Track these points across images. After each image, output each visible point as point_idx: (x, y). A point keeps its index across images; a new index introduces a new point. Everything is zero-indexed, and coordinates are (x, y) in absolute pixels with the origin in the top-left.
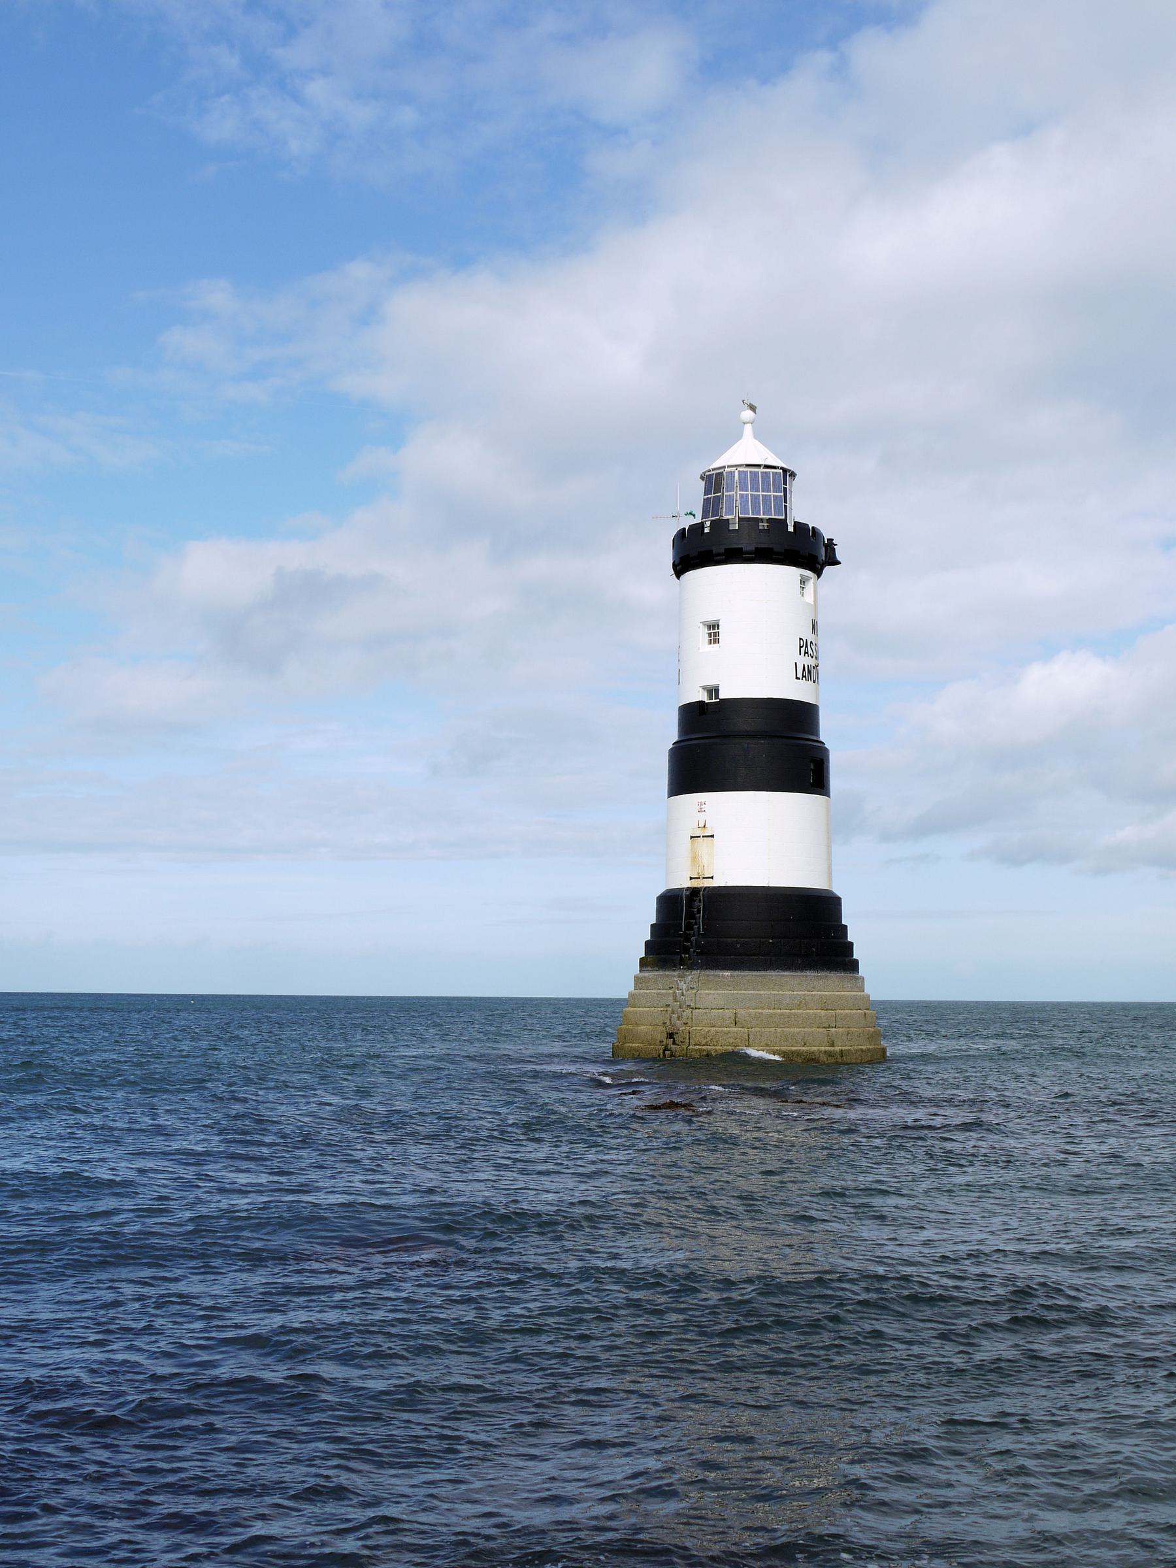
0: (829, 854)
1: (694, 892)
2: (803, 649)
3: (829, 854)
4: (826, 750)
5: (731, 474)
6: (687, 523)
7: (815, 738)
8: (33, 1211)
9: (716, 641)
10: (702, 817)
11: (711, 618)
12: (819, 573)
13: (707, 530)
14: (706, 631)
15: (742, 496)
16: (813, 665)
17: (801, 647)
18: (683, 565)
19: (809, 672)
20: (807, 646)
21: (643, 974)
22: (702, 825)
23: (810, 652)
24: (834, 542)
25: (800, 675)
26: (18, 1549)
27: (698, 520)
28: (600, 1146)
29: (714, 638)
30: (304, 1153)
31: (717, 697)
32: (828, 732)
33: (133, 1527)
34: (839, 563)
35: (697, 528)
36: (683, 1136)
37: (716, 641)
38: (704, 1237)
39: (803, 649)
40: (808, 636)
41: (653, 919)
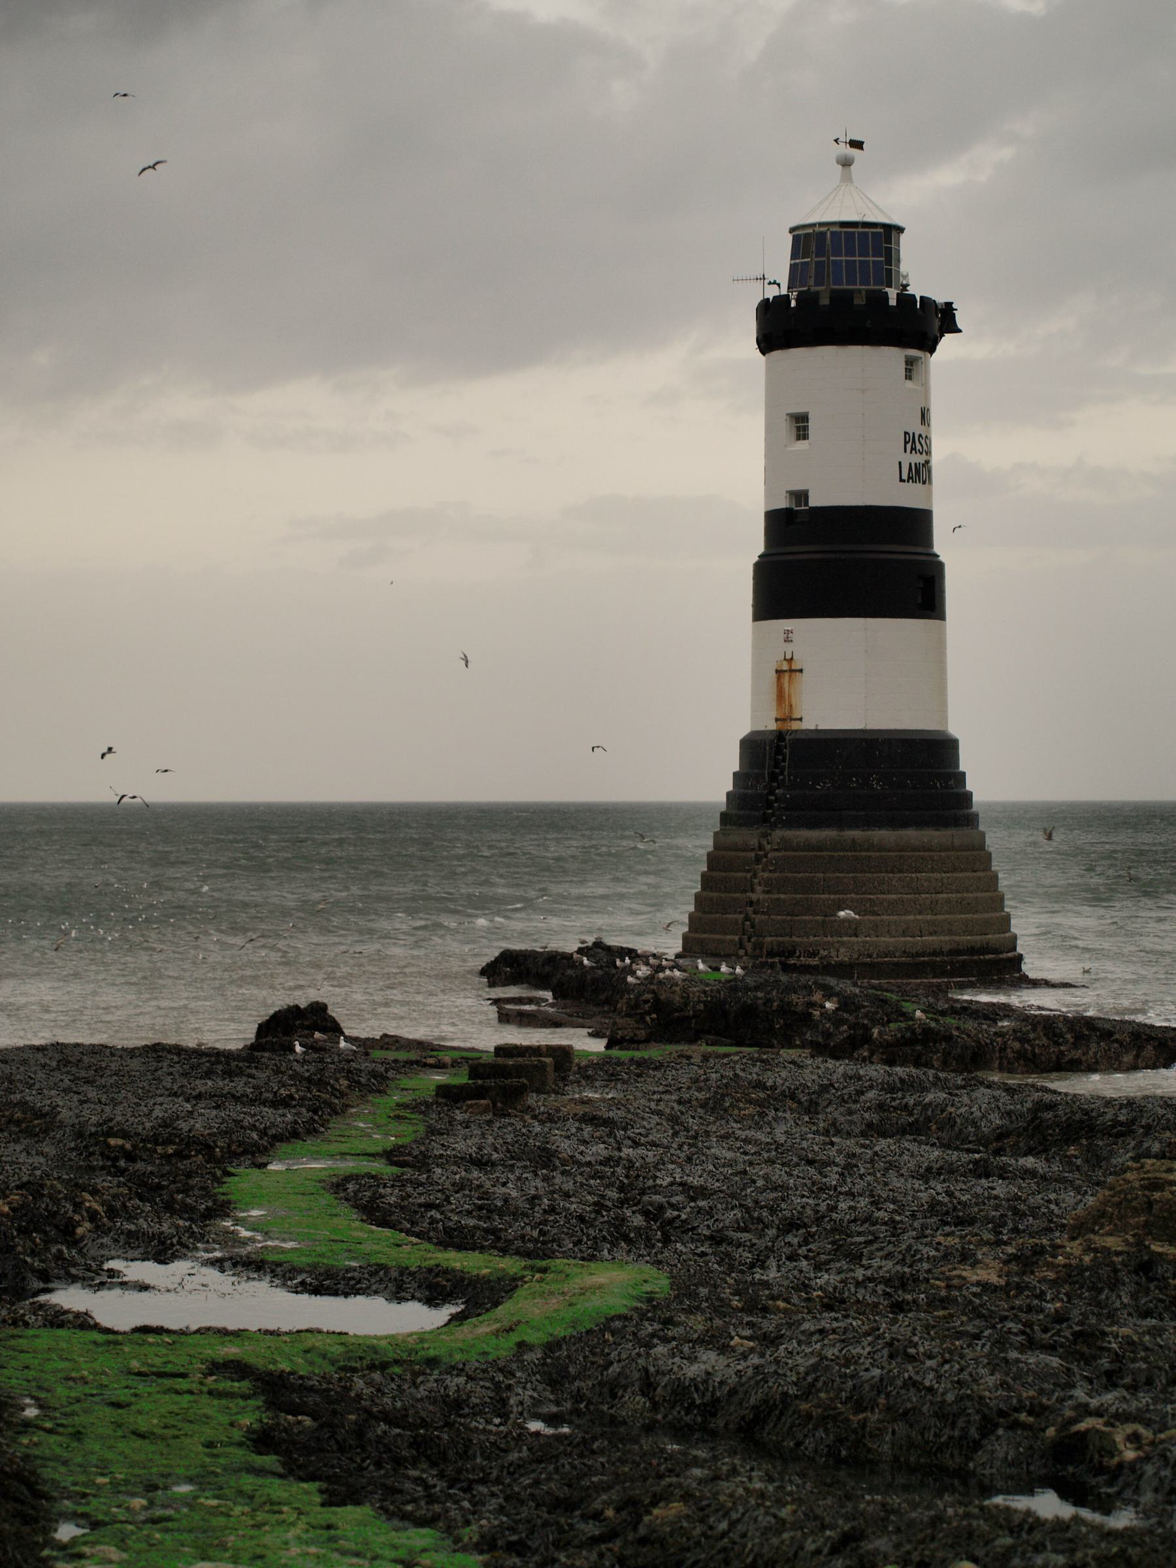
1: (780, 735)
2: (909, 446)
4: (940, 566)
5: (823, 234)
6: (771, 293)
7: (920, 550)
10: (789, 648)
12: (949, 305)
13: (793, 304)
15: (835, 262)
16: (922, 462)
17: (906, 443)
19: (918, 472)
21: (705, 894)
22: (788, 657)
23: (918, 447)
24: (954, 306)
25: (905, 477)
26: (528, 1025)
27: (784, 291)
30: (619, 1006)
31: (806, 504)
32: (943, 545)
34: (960, 331)
35: (782, 300)
36: (413, 1390)
40: (916, 428)
41: (736, 767)
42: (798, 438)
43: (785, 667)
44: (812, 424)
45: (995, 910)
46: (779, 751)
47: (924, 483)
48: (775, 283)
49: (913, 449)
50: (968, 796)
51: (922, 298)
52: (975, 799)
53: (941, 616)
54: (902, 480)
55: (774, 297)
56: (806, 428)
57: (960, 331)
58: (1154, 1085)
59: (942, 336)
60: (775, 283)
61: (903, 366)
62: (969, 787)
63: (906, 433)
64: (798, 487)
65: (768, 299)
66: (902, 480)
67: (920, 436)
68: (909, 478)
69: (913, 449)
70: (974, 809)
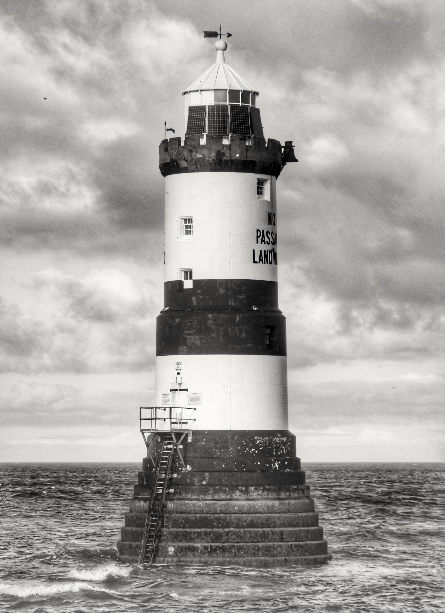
0: (223, 54)
2: (260, 239)
3: (223, 54)
4: (284, 318)
8: (413, 565)
9: (190, 232)
11: (187, 215)
14: (184, 224)
17: (258, 237)
18: (165, 174)
19: (266, 256)
20: (263, 236)
21: (129, 528)
23: (267, 239)
24: (293, 144)
25: (257, 259)
28: (401, 530)
29: (189, 230)
33: (81, 601)
34: (297, 161)
37: (190, 232)
38: (285, 577)
39: (260, 239)
42: (186, 233)
43: (177, 387)
44: (194, 224)
45: (227, 109)
46: (291, 547)
47: (271, 263)
48: (171, 130)
49: (263, 241)
50: (299, 460)
51: (269, 140)
52: (302, 461)
53: (286, 356)
54: (255, 262)
55: (171, 139)
56: (190, 227)
57: (297, 161)
58: (327, 574)
59: (284, 164)
60: (171, 130)
61: (256, 186)
62: (298, 455)
63: (258, 230)
64: (187, 267)
65: (167, 140)
66: (255, 262)
67: (268, 232)
68: (260, 260)
69: (263, 241)
70: (301, 470)
